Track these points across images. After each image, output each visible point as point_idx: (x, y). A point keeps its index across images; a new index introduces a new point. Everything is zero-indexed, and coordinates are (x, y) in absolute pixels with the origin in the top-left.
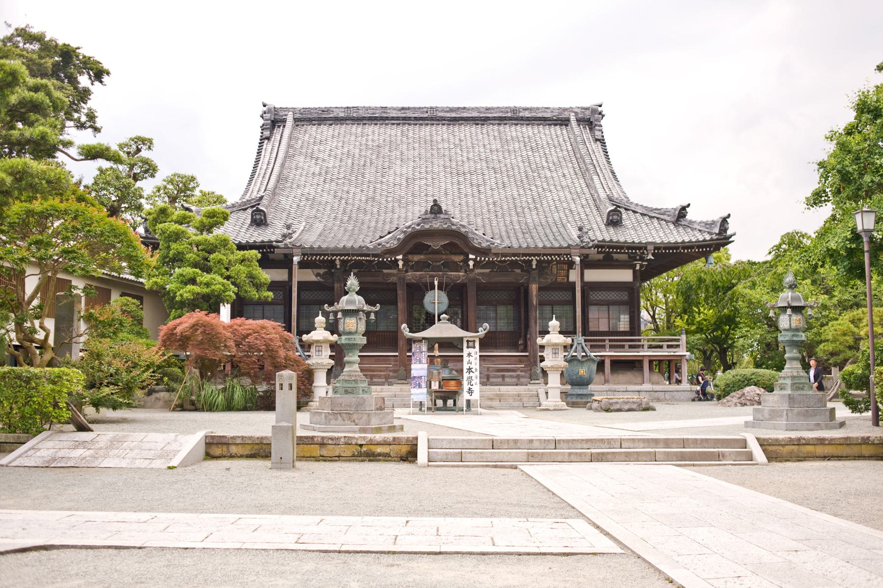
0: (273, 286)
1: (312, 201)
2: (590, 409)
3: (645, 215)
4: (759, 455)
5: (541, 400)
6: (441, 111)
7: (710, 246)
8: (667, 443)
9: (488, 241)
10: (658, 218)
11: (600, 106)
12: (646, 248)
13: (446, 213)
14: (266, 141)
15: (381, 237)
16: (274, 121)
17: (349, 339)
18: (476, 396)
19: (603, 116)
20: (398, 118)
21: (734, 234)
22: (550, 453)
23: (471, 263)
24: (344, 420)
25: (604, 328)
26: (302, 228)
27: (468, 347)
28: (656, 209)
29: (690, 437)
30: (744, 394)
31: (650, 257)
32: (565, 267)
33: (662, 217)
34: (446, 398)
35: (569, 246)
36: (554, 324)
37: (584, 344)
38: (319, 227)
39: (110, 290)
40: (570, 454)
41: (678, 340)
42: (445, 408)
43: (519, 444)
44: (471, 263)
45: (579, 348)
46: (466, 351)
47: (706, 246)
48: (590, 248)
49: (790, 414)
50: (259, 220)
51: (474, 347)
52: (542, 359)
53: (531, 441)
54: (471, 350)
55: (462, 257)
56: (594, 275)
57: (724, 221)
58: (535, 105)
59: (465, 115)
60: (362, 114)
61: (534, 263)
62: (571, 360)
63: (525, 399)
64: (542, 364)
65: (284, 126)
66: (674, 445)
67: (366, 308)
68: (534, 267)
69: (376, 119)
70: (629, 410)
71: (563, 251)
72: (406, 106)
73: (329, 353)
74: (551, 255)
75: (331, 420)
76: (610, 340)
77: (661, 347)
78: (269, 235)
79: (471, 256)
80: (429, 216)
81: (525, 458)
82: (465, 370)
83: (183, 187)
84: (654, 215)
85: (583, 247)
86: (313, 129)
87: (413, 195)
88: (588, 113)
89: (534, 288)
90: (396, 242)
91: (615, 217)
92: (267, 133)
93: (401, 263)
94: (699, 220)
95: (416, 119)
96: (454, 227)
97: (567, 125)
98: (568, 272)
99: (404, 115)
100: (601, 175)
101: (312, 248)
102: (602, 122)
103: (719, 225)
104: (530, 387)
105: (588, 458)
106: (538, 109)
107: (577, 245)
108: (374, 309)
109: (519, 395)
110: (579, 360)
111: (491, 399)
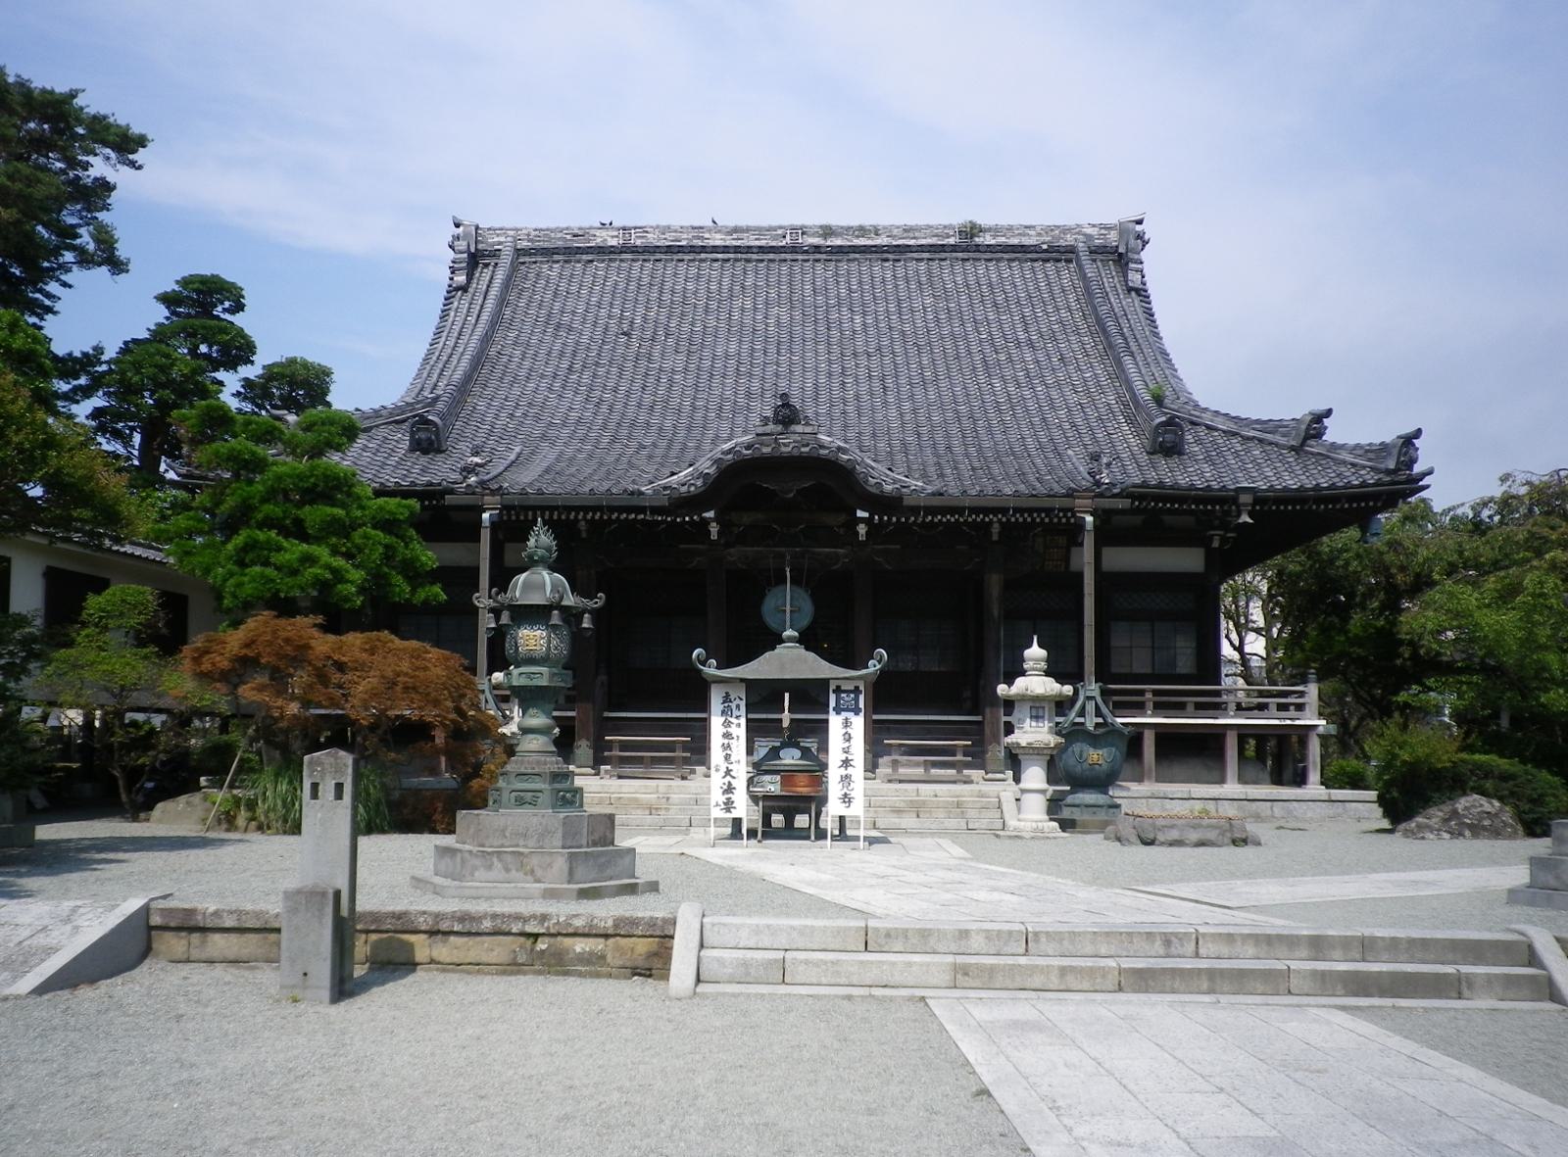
0: (440, 575)
3: (1235, 434)
5: (1007, 816)
7: (1375, 496)
8: (1318, 945)
9: (895, 481)
10: (1261, 441)
11: (1140, 222)
12: (1234, 500)
15: (673, 474)
16: (475, 258)
17: (529, 675)
18: (857, 809)
19: (1145, 243)
20: (725, 249)
21: (1430, 472)
22: (1013, 967)
23: (862, 529)
24: (507, 870)
25: (1141, 666)
26: (513, 457)
28: (1258, 421)
29: (1379, 933)
30: (1455, 812)
31: (1245, 518)
32: (1062, 541)
33: (1269, 437)
34: (790, 810)
35: (1071, 494)
36: (1035, 652)
37: (1099, 699)
38: (547, 456)
41: (1302, 694)
42: (789, 832)
43: (932, 941)
44: (862, 529)
45: (1090, 707)
47: (1365, 497)
48: (1114, 496)
50: (427, 438)
52: (1009, 729)
53: (964, 934)
55: (842, 518)
56: (1126, 559)
57: (1409, 441)
58: (1004, 222)
60: (653, 239)
61: (996, 528)
62: (1073, 734)
63: (972, 813)
64: (1010, 739)
66: (1337, 954)
67: (570, 600)
68: (995, 537)
69: (681, 249)
70: (1201, 844)
71: (1057, 503)
72: (742, 223)
74: (1030, 511)
75: (475, 868)
76: (1156, 693)
77: (1262, 707)
78: (441, 471)
79: (860, 514)
80: (771, 427)
81: (947, 978)
83: (302, 385)
84: (1251, 433)
85: (1101, 495)
87: (749, 395)
88: (1113, 236)
89: (994, 583)
90: (699, 483)
91: (1168, 437)
92: (461, 279)
93: (714, 528)
94: (1352, 442)
95: (762, 249)
96: (822, 452)
98: (1068, 551)
101: (523, 493)
103: (1395, 452)
105: (1111, 981)
106: (1010, 228)
108: (591, 604)
109: (959, 805)
110: (1087, 733)
111: (898, 811)
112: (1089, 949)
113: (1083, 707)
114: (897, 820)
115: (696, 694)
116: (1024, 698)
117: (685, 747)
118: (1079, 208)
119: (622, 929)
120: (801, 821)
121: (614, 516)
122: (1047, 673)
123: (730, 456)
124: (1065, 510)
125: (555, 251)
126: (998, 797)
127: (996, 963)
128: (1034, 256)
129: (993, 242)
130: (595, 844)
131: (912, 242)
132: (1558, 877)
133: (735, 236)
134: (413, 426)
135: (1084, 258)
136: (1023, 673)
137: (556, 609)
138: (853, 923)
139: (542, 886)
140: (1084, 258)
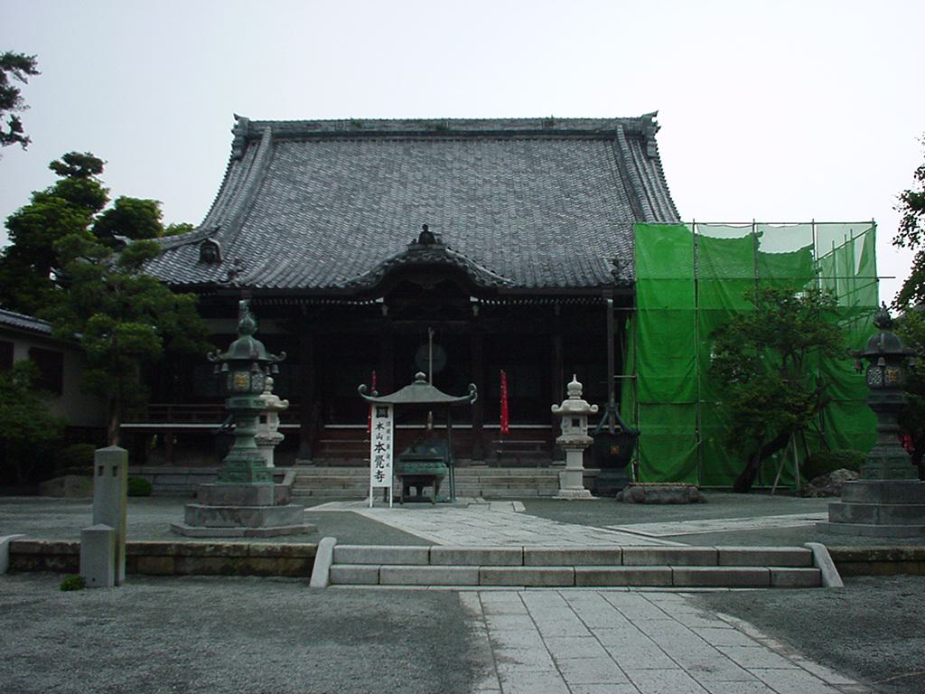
1: (283, 233)
2: (621, 500)
4: (833, 578)
6: (455, 125)
11: (655, 115)
13: (440, 243)
14: (236, 162)
16: (248, 136)
20: (401, 133)
23: (475, 309)
24: (225, 519)
27: (378, 416)
30: (546, 687)
39: (12, 345)
40: (542, 573)
44: (475, 309)
46: (375, 421)
49: (882, 513)
50: (210, 256)
51: (387, 416)
54: (382, 420)
59: (485, 129)
61: (557, 309)
65: (259, 145)
70: (672, 502)
73: (278, 424)
74: (577, 297)
78: (218, 275)
81: (475, 580)
82: (373, 447)
86: (294, 148)
92: (238, 152)
93: (385, 310)
97: (612, 140)
99: (409, 129)
100: (652, 199)
102: (657, 137)
104: (550, 470)
107: (611, 284)
110: (610, 434)
112: (560, 561)
113: (608, 418)
114: (495, 490)
115: (361, 413)
116: (568, 414)
117: (543, 447)
118: (630, 109)
119: (286, 553)
120: (428, 491)
121: (323, 301)
122: (582, 398)
123: (392, 264)
124: (598, 297)
125: (298, 135)
126: (558, 475)
127: (497, 569)
128: (592, 137)
129: (565, 129)
130: (279, 504)
131: (516, 129)
132: (843, 515)
133: (407, 125)
134: (202, 245)
135: (622, 138)
136: (567, 398)
137: (880, 356)
138: (424, 548)
139: (245, 529)
140: (622, 138)
